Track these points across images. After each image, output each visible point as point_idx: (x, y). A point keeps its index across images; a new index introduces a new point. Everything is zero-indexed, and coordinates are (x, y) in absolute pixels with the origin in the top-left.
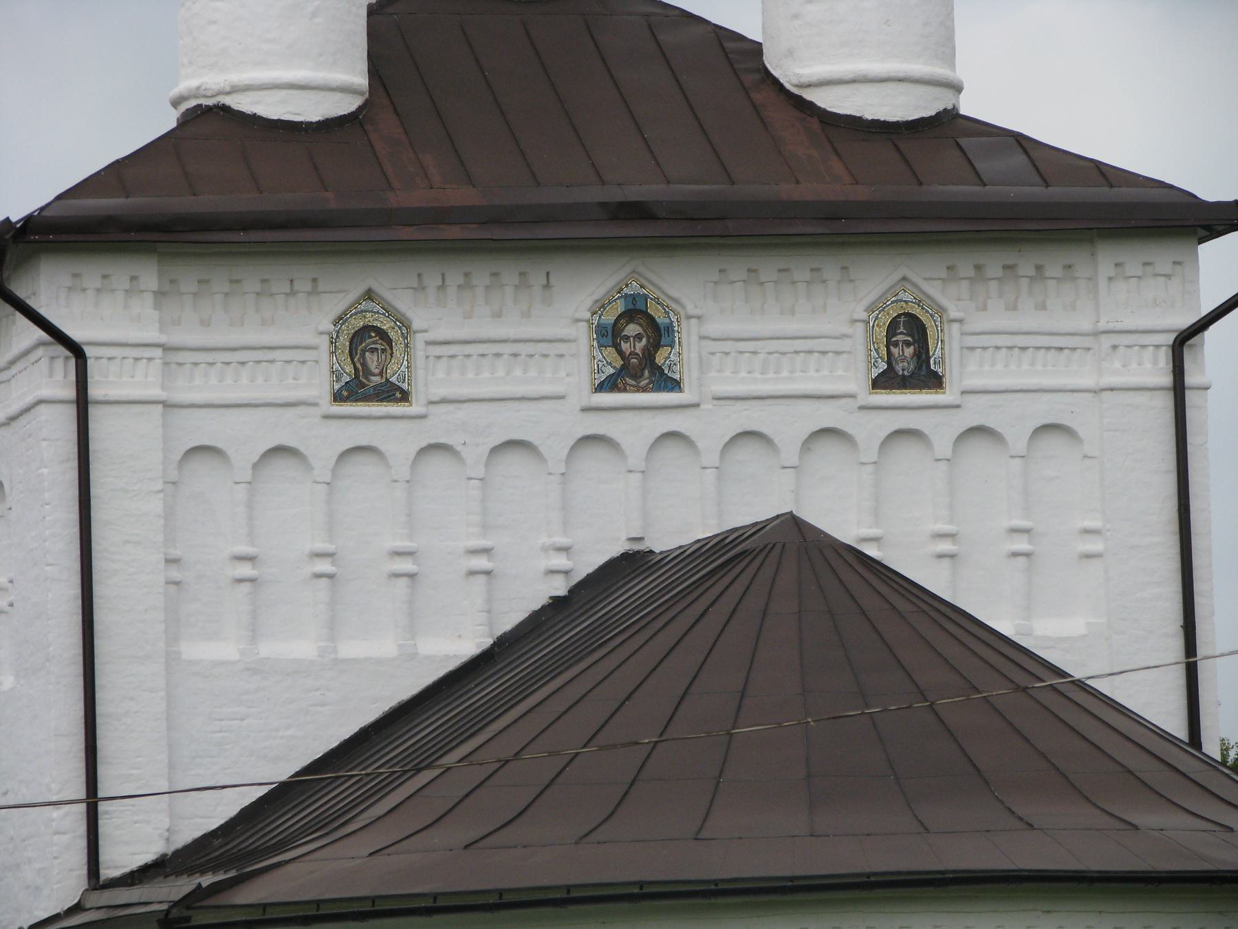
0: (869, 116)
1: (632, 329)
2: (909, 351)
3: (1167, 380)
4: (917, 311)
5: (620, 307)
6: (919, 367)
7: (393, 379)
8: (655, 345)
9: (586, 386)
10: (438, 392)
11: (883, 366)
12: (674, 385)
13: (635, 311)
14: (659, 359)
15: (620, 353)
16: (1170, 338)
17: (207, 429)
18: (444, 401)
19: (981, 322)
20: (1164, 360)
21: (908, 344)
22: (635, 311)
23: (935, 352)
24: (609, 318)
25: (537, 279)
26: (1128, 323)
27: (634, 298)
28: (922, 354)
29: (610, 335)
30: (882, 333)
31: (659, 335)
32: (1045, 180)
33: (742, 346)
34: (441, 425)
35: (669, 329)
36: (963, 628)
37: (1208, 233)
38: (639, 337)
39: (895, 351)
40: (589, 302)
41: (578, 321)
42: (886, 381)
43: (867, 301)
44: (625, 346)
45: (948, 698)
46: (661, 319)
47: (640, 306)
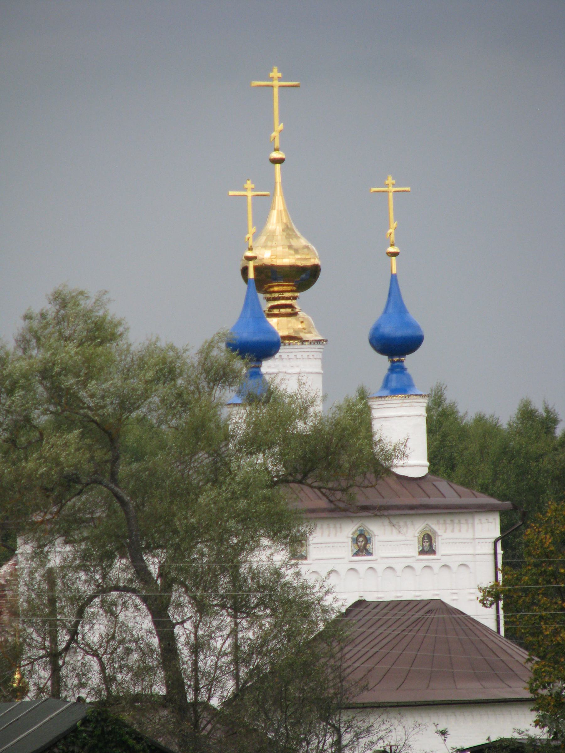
0: (410, 476)
1: (361, 539)
2: (428, 544)
3: (492, 552)
4: (429, 533)
5: (358, 533)
6: (430, 548)
7: (303, 554)
8: (366, 544)
9: (351, 555)
10: (444, 552)
11: (421, 548)
12: (371, 554)
13: (362, 534)
14: (367, 547)
15: (358, 545)
16: (493, 540)
17: (391, 563)
18: (316, 560)
19: (445, 536)
20: (491, 546)
21: (427, 542)
22: (362, 534)
23: (434, 545)
24: (355, 536)
25: (338, 526)
26: (483, 536)
27: (361, 531)
28: (431, 545)
29: (355, 541)
30: (421, 539)
31: (367, 541)
32: (459, 495)
33: (387, 543)
34: (445, 560)
35: (370, 539)
36: (367, 637)
37: (323, 503)
38: (362, 541)
39: (424, 544)
40: (351, 532)
41: (348, 537)
42: (422, 552)
43: (418, 531)
44: (359, 544)
45: (46, 723)
46: (368, 536)
47: (363, 533)
